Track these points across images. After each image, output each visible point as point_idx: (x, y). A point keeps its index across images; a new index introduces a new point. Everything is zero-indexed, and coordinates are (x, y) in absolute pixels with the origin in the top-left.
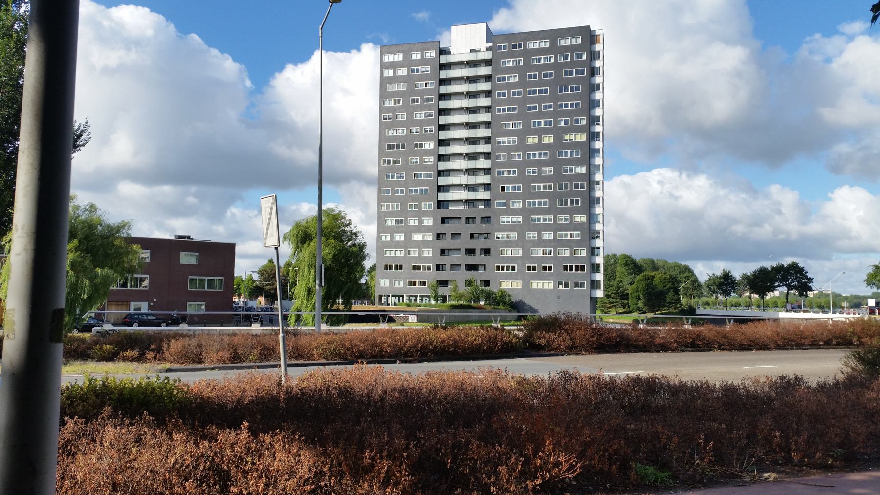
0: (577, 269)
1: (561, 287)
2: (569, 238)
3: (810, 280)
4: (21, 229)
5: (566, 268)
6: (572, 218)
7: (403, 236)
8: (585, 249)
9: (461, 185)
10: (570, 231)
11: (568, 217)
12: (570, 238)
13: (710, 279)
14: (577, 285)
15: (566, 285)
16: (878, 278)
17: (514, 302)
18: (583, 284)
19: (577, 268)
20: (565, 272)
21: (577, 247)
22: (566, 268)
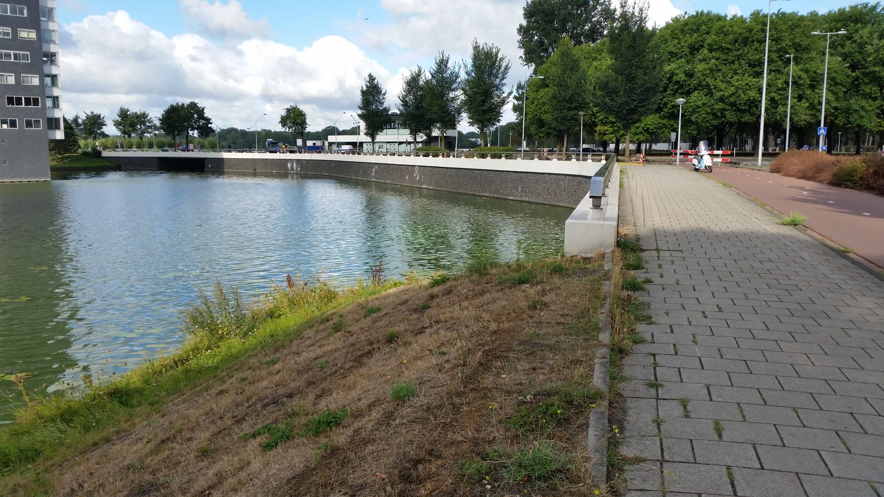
0: (28, 101)
1: (5, 126)
2: (12, 60)
3: (697, 13)
4: (568, 158)
5: (10, 101)
6: (15, 33)
7: (13, 78)
8: (13, 75)
9: (859, 423)
10: (13, 50)
11: (9, 30)
12: (14, 59)
13: (87, 118)
14: (29, 124)
15: (13, 124)
16: (464, 489)
17: (671, 22)
18: (37, 122)
19: (28, 101)
20: (10, 106)
21: (26, 73)
22: (10, 101)
